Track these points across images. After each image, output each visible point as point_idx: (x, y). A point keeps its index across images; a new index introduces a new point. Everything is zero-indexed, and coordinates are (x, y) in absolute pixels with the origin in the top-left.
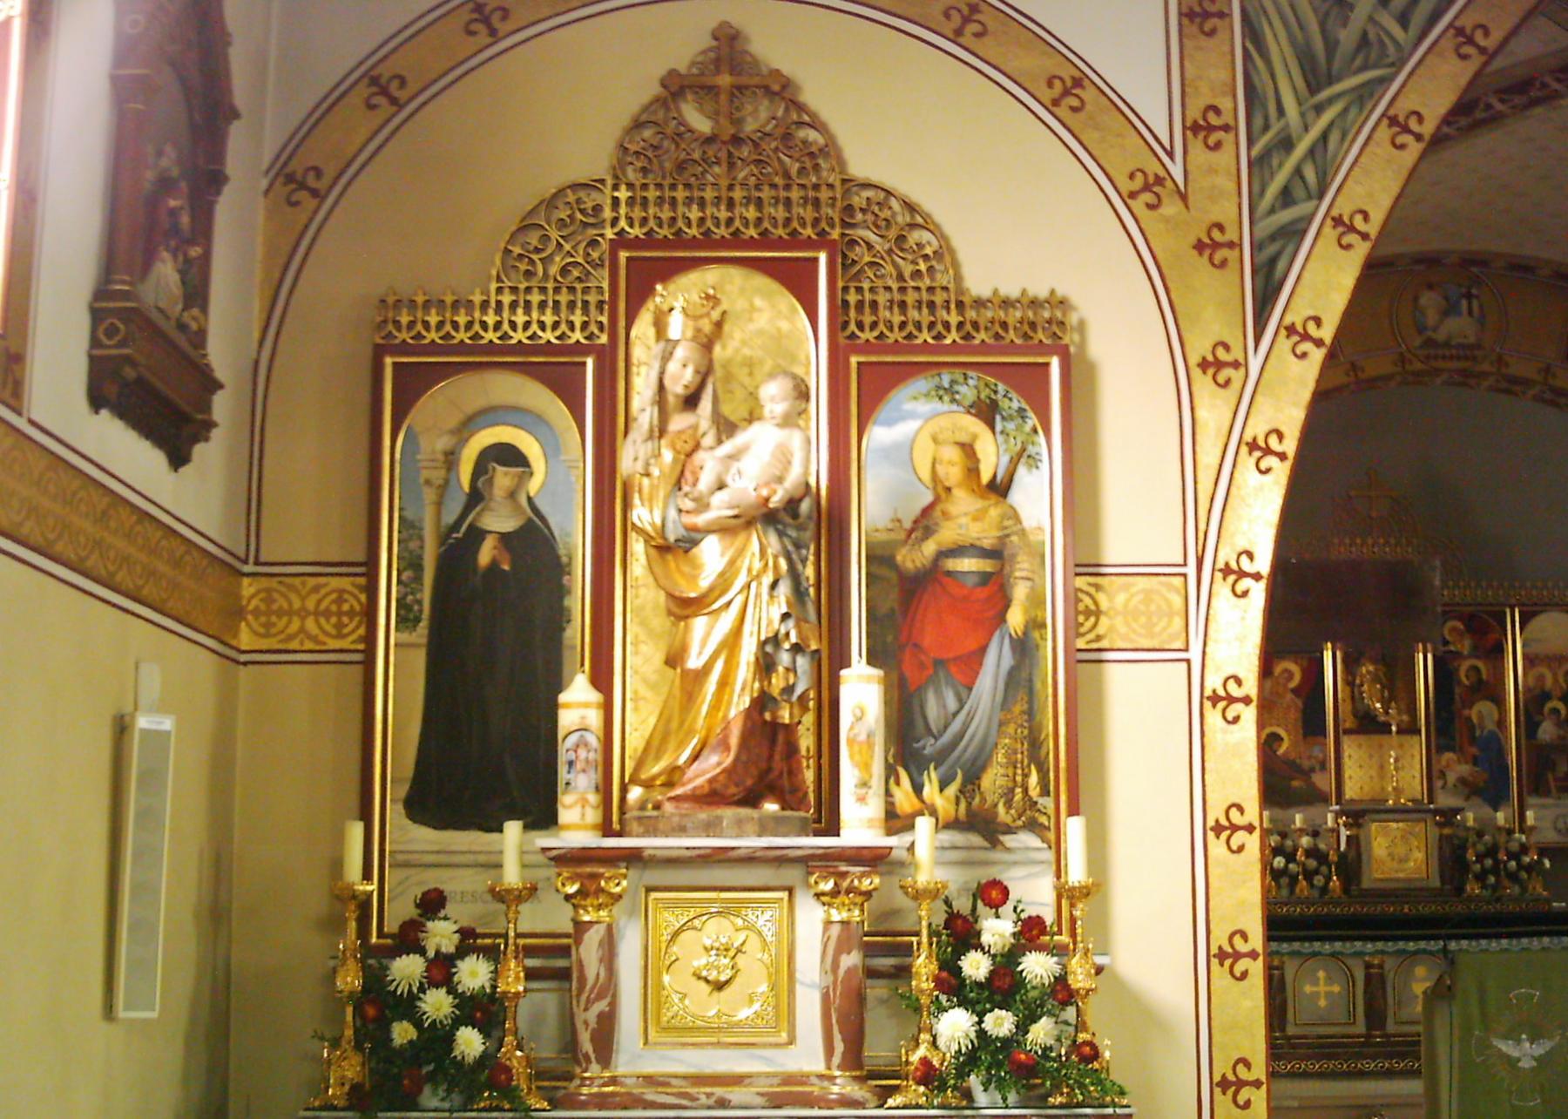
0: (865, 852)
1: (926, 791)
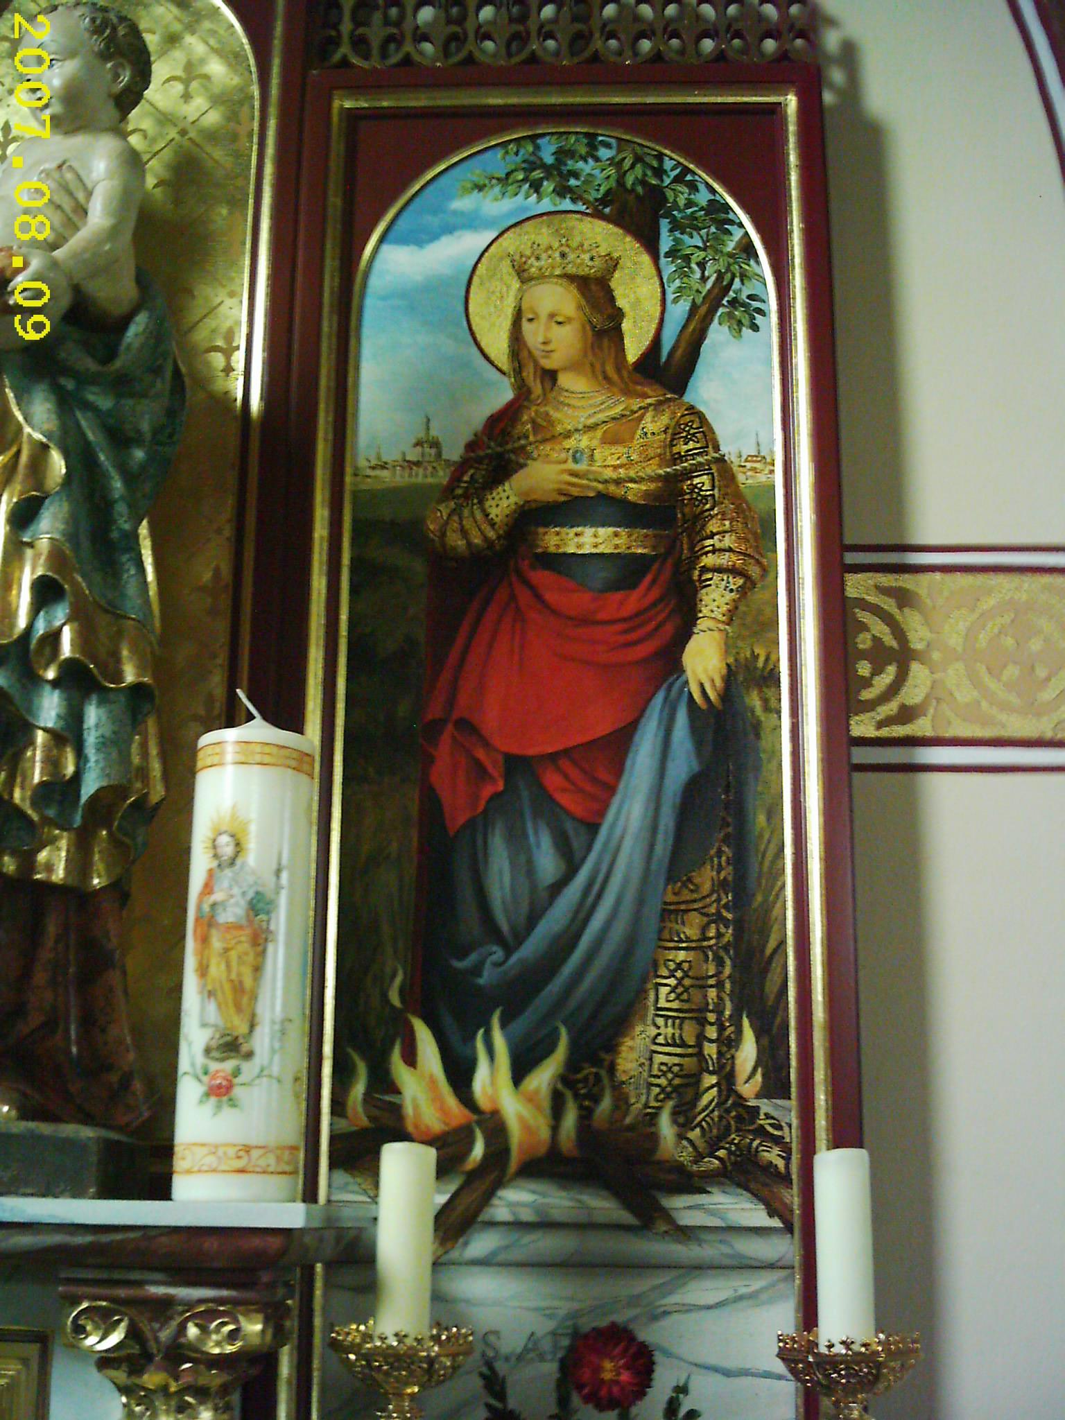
0: (211, 1244)
1: (481, 1081)
